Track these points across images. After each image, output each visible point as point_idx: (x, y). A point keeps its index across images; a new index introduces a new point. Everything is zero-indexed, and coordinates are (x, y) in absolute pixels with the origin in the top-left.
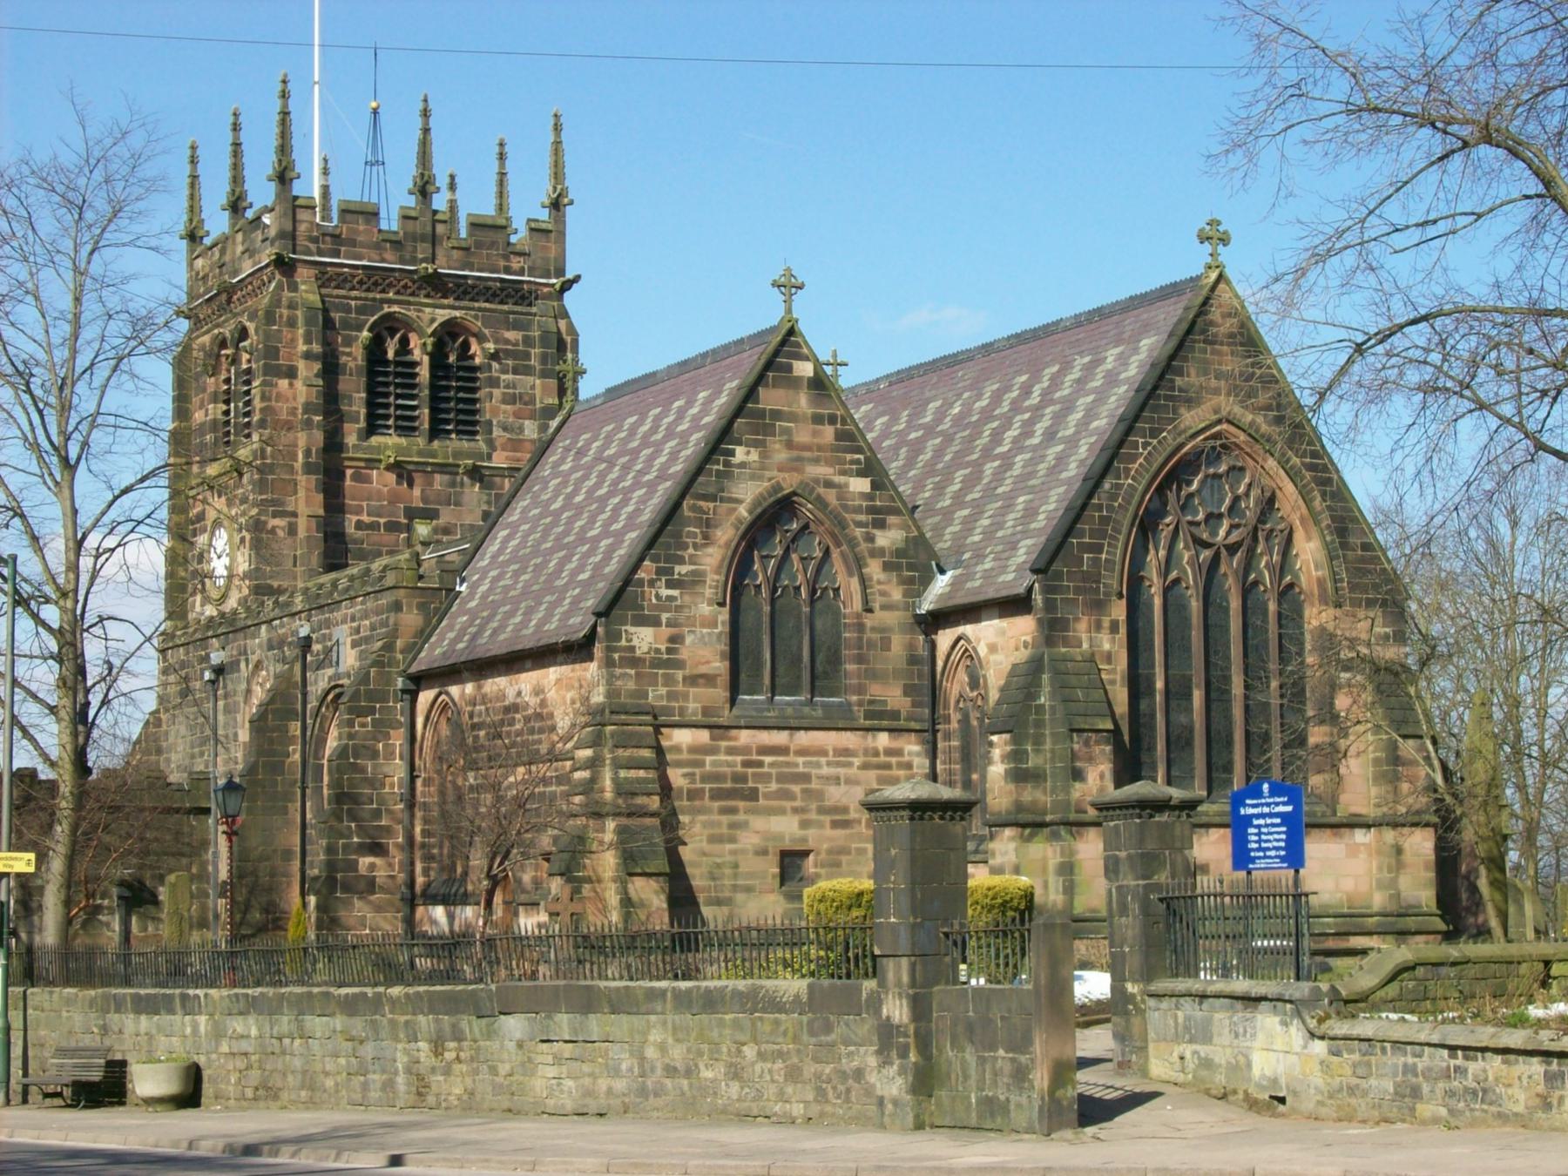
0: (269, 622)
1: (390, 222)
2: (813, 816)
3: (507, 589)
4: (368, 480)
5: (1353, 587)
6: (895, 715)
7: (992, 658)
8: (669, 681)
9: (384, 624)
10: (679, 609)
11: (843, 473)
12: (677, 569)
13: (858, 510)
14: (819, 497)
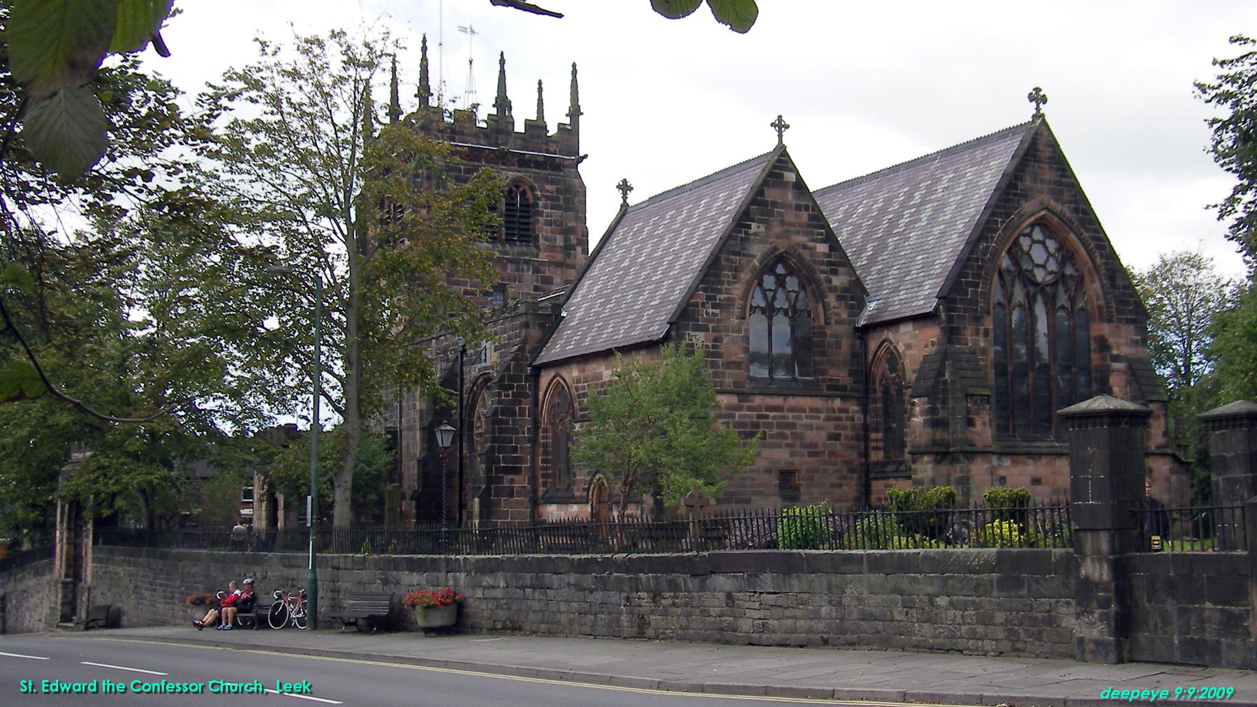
0: (437, 338)
2: (798, 449)
5: (1119, 312)
6: (844, 388)
9: (517, 336)
10: (719, 321)
11: (813, 240)
12: (718, 297)
13: (822, 263)
14: (799, 255)
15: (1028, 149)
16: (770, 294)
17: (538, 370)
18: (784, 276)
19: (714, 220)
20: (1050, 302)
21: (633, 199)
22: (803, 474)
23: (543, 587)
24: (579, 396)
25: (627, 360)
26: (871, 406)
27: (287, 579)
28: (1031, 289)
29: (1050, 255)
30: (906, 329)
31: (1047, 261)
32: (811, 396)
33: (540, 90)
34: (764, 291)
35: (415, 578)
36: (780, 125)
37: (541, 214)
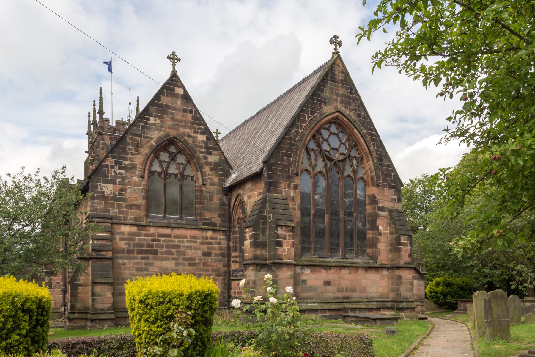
6: (214, 224)
8: (119, 206)
10: (124, 178)
12: (124, 162)
13: (201, 147)
26: (232, 236)
28: (329, 164)
33: (101, 93)
34: (161, 162)
36: (174, 58)
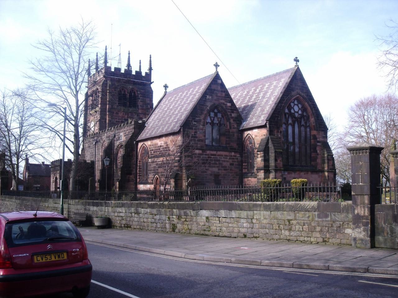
1: (123, 71)
3: (157, 125)
4: (118, 114)
6: (235, 149)
7: (256, 138)
8: (195, 140)
9: (131, 132)
12: (196, 118)
15: (293, 76)
16: (212, 118)
17: (138, 142)
18: (217, 113)
19: (195, 95)
20: (300, 123)
21: (168, 90)
22: (222, 176)
23: (138, 213)
24: (150, 150)
25: (167, 138)
27: (55, 207)
29: (299, 109)
30: (256, 131)
31: (299, 111)
32: (225, 151)
33: (140, 63)
34: (211, 118)
35: (95, 208)
37: (139, 99)
